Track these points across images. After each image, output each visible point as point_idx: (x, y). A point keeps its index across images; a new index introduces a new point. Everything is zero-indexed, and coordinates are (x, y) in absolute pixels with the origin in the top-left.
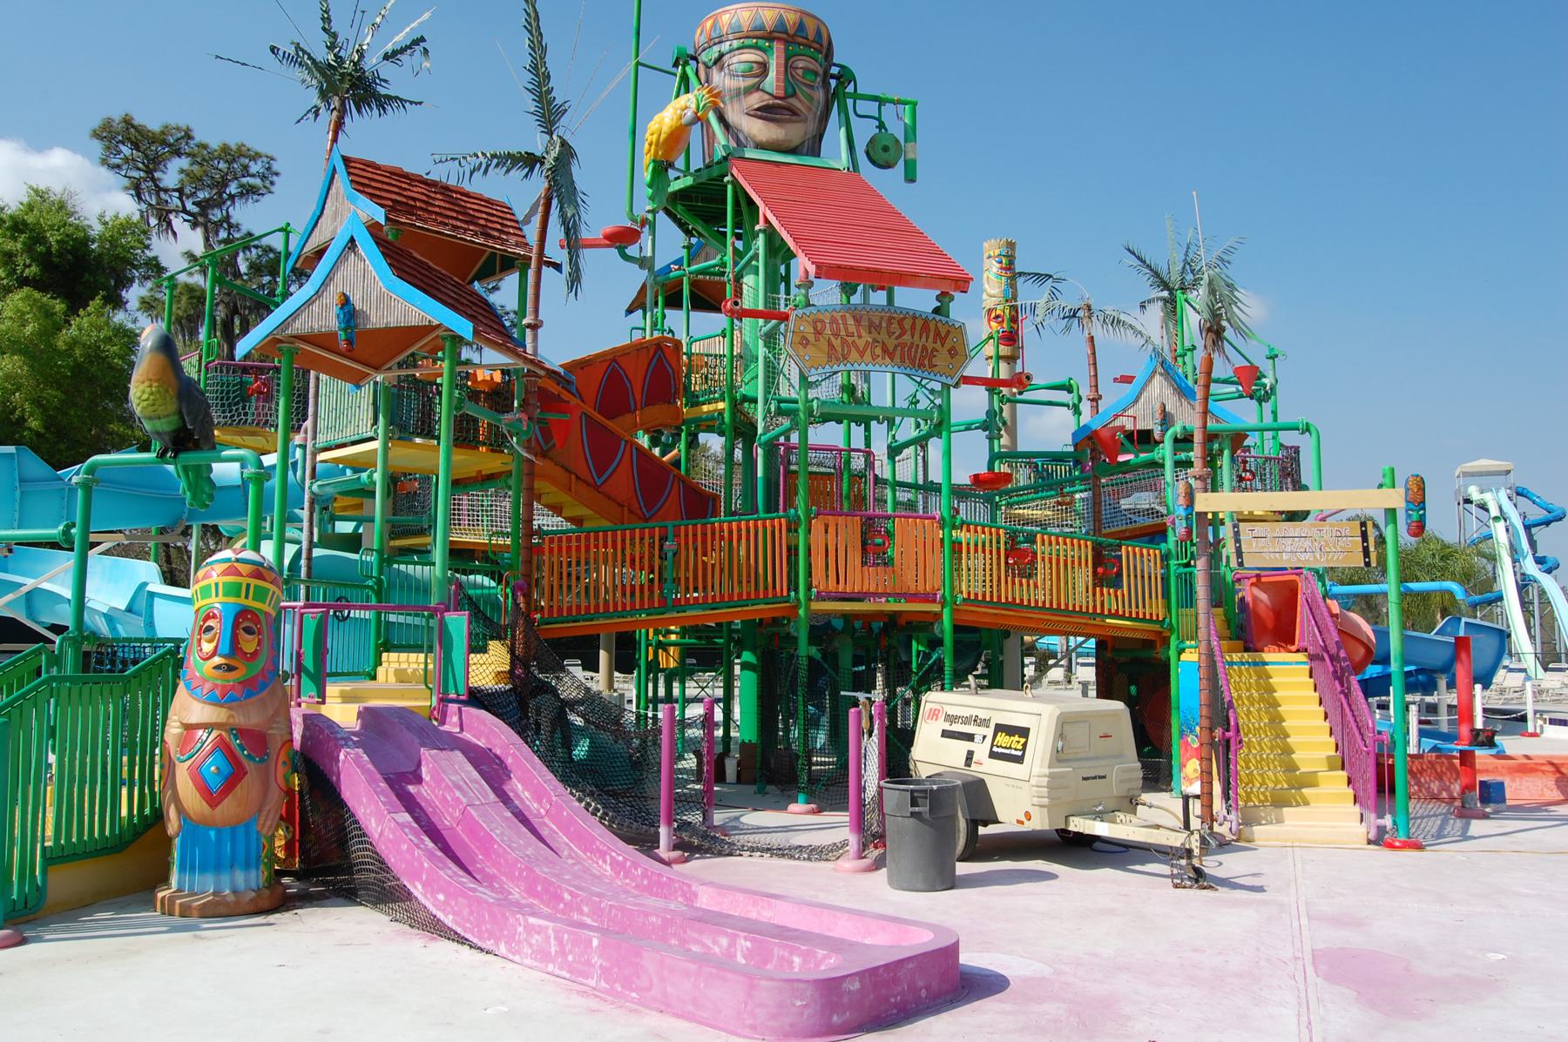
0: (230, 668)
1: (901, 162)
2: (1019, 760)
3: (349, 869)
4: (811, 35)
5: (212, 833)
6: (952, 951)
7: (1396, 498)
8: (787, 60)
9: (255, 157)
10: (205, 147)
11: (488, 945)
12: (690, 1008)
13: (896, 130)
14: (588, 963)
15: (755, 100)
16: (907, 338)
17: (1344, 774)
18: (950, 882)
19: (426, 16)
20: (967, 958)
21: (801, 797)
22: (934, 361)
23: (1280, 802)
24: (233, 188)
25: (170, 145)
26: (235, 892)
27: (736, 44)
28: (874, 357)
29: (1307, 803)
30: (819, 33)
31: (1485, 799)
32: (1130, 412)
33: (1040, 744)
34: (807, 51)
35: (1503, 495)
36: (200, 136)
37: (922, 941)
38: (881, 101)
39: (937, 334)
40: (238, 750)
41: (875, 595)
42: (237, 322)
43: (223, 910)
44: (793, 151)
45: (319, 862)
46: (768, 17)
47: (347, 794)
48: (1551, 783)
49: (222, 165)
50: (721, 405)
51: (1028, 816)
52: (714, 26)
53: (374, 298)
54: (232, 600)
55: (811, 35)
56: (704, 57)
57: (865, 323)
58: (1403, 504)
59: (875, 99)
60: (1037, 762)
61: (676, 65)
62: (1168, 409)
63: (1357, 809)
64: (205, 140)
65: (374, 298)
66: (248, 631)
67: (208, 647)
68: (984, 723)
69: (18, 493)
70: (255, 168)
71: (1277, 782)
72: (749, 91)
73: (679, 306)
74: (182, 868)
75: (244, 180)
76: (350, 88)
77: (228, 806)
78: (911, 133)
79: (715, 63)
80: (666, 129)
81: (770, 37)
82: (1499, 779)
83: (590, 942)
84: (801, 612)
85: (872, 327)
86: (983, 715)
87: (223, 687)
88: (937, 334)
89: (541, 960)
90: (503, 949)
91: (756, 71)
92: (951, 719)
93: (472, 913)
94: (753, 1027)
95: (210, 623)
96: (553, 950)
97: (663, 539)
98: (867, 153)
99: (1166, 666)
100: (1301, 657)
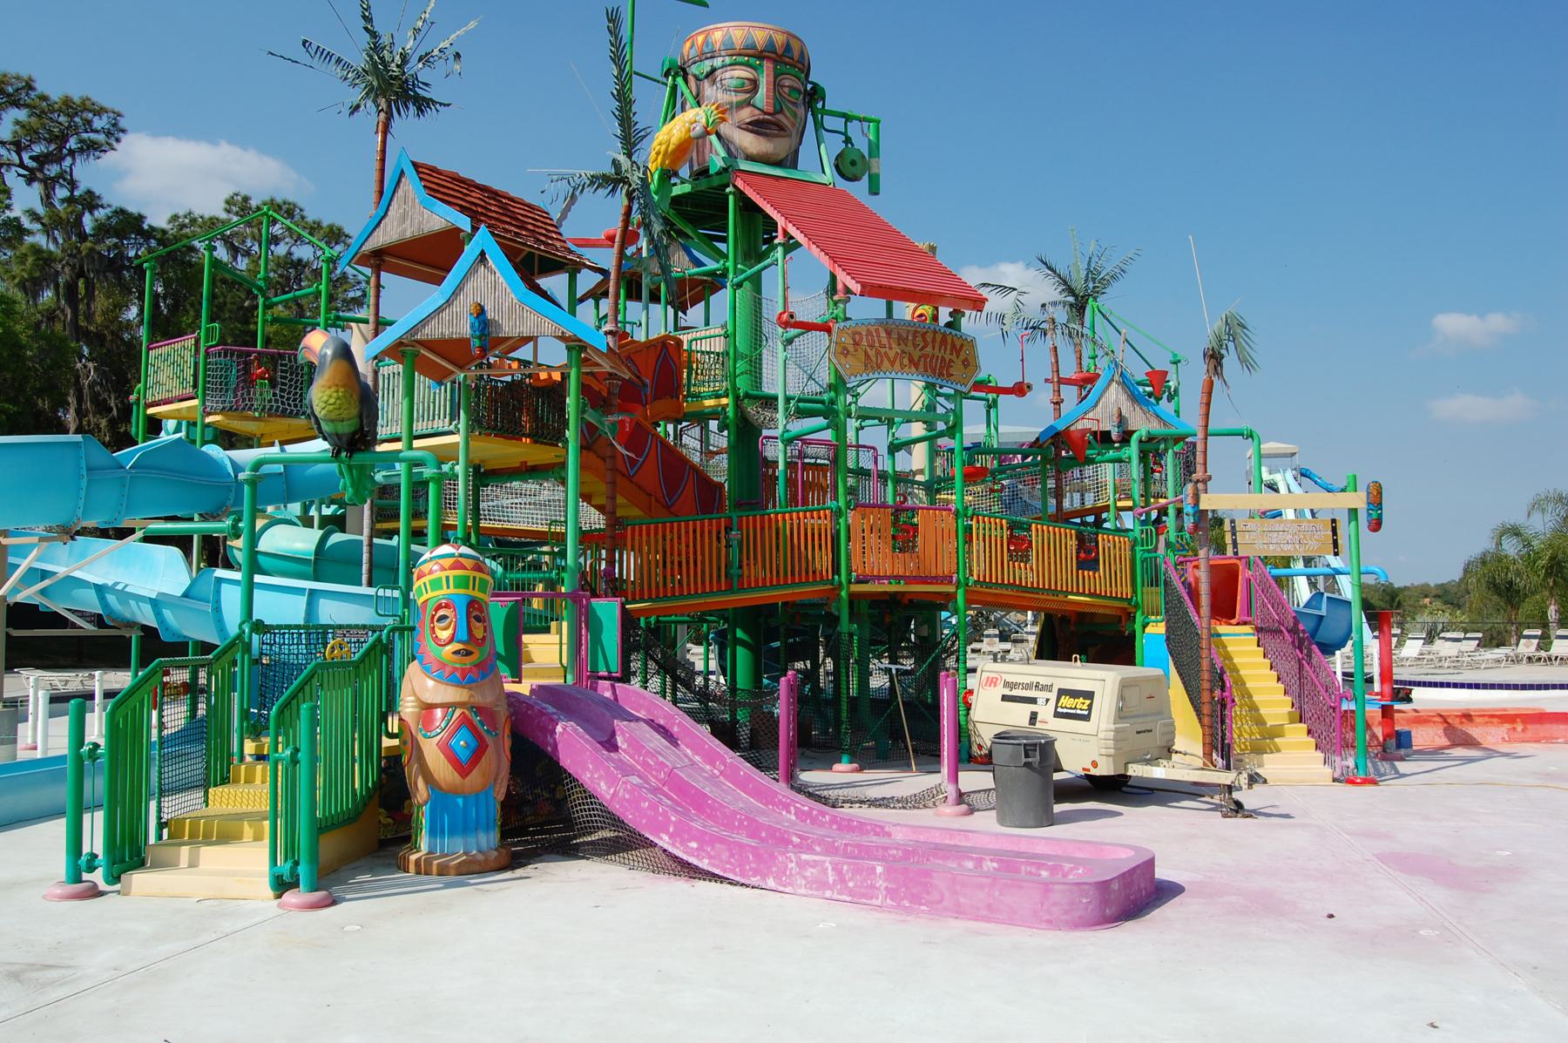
0: (468, 653)
1: (866, 178)
2: (1086, 718)
3: (569, 823)
4: (796, 55)
5: (460, 801)
6: (1150, 864)
7: (1359, 500)
8: (775, 77)
9: (99, 112)
10: (44, 98)
11: (755, 880)
12: (984, 913)
13: (861, 145)
14: (873, 887)
15: (746, 114)
16: (929, 350)
17: (1304, 726)
18: (1051, 820)
19: (472, 25)
20: (1161, 873)
21: (845, 758)
22: (952, 371)
23: (1258, 750)
24: (72, 143)
25: (9, 95)
26: (480, 851)
27: (728, 60)
28: (903, 366)
29: (1278, 751)
30: (802, 53)
31: (1399, 746)
32: (1091, 415)
33: (1106, 706)
34: (792, 71)
35: (1289, 475)
36: (41, 87)
37: (1126, 860)
38: (847, 118)
39: (953, 346)
40: (479, 726)
41: (879, 578)
42: (81, 283)
43: (477, 868)
44: (778, 164)
45: (540, 818)
46: (760, 37)
47: (566, 761)
48: (1441, 732)
49: (62, 119)
50: (724, 401)
51: (1095, 764)
52: (705, 41)
53: (505, 308)
54: (462, 591)
55: (796, 55)
56: (694, 70)
57: (895, 336)
58: (1365, 506)
59: (844, 115)
60: (1104, 719)
61: (667, 75)
62: (490, 315)
63: (1320, 755)
64: (47, 93)
65: (505, 308)
66: (478, 619)
67: (444, 635)
68: (1048, 688)
69: (84, 483)
70: (98, 123)
71: (1251, 734)
72: (740, 106)
73: (639, 298)
74: (433, 832)
75: (85, 136)
76: (394, 89)
77: (475, 776)
78: (874, 149)
79: (707, 76)
80: (674, 141)
81: (760, 56)
82: (1406, 728)
83: (873, 869)
84: (844, 594)
85: (901, 340)
86: (1043, 681)
87: (463, 670)
88: (953, 346)
89: (817, 889)
90: (771, 883)
91: (748, 87)
92: (1007, 684)
93: (732, 855)
94: (1049, 922)
95: (441, 612)
96: (831, 880)
97: (728, 529)
98: (837, 167)
99: (1133, 636)
100: (1247, 629)
